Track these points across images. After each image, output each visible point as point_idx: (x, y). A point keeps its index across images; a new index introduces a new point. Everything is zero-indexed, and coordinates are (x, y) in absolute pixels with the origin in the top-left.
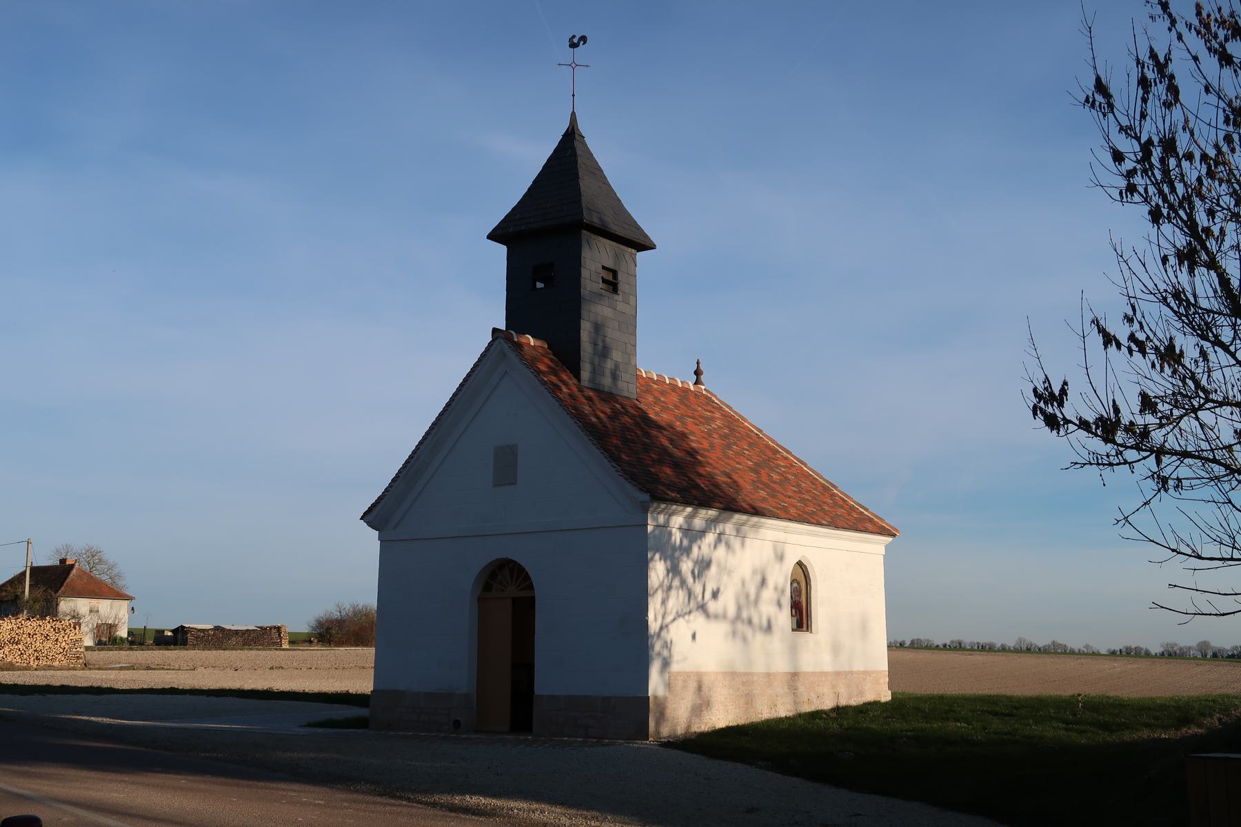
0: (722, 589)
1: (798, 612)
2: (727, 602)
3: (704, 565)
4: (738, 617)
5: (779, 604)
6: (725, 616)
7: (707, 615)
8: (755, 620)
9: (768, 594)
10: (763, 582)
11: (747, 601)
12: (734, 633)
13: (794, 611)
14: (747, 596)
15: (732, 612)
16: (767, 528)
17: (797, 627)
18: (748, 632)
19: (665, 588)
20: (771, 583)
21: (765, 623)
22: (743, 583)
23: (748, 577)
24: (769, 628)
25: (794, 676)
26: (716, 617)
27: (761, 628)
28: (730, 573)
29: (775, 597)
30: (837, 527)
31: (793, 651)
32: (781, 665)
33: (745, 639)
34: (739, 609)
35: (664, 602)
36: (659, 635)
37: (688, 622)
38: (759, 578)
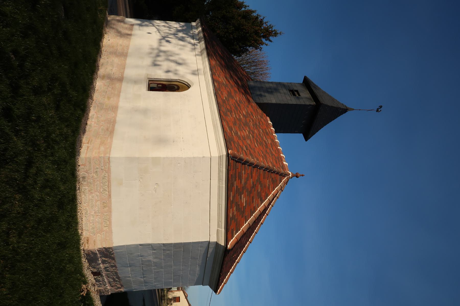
0: (171, 44)
1: (160, 88)
2: (166, 47)
3: (182, 39)
4: (161, 51)
5: (168, 71)
6: (161, 46)
7: (161, 40)
8: (159, 59)
9: (173, 66)
10: (179, 64)
11: (168, 55)
12: (153, 49)
13: (160, 86)
14: (171, 56)
15: (163, 48)
16: (202, 59)
17: (150, 87)
18: (153, 55)
19: (169, 27)
20: (179, 68)
21: (158, 63)
22: (178, 54)
23: (181, 56)
24: (155, 64)
25: (121, 79)
26: (160, 43)
27: (155, 61)
28: (181, 49)
29: (171, 69)
30: (216, 94)
31: (136, 82)
32: (129, 72)
33: (151, 53)
34: (164, 52)
35: (164, 26)
36: (151, 23)
37: (156, 32)
38: (180, 61)
